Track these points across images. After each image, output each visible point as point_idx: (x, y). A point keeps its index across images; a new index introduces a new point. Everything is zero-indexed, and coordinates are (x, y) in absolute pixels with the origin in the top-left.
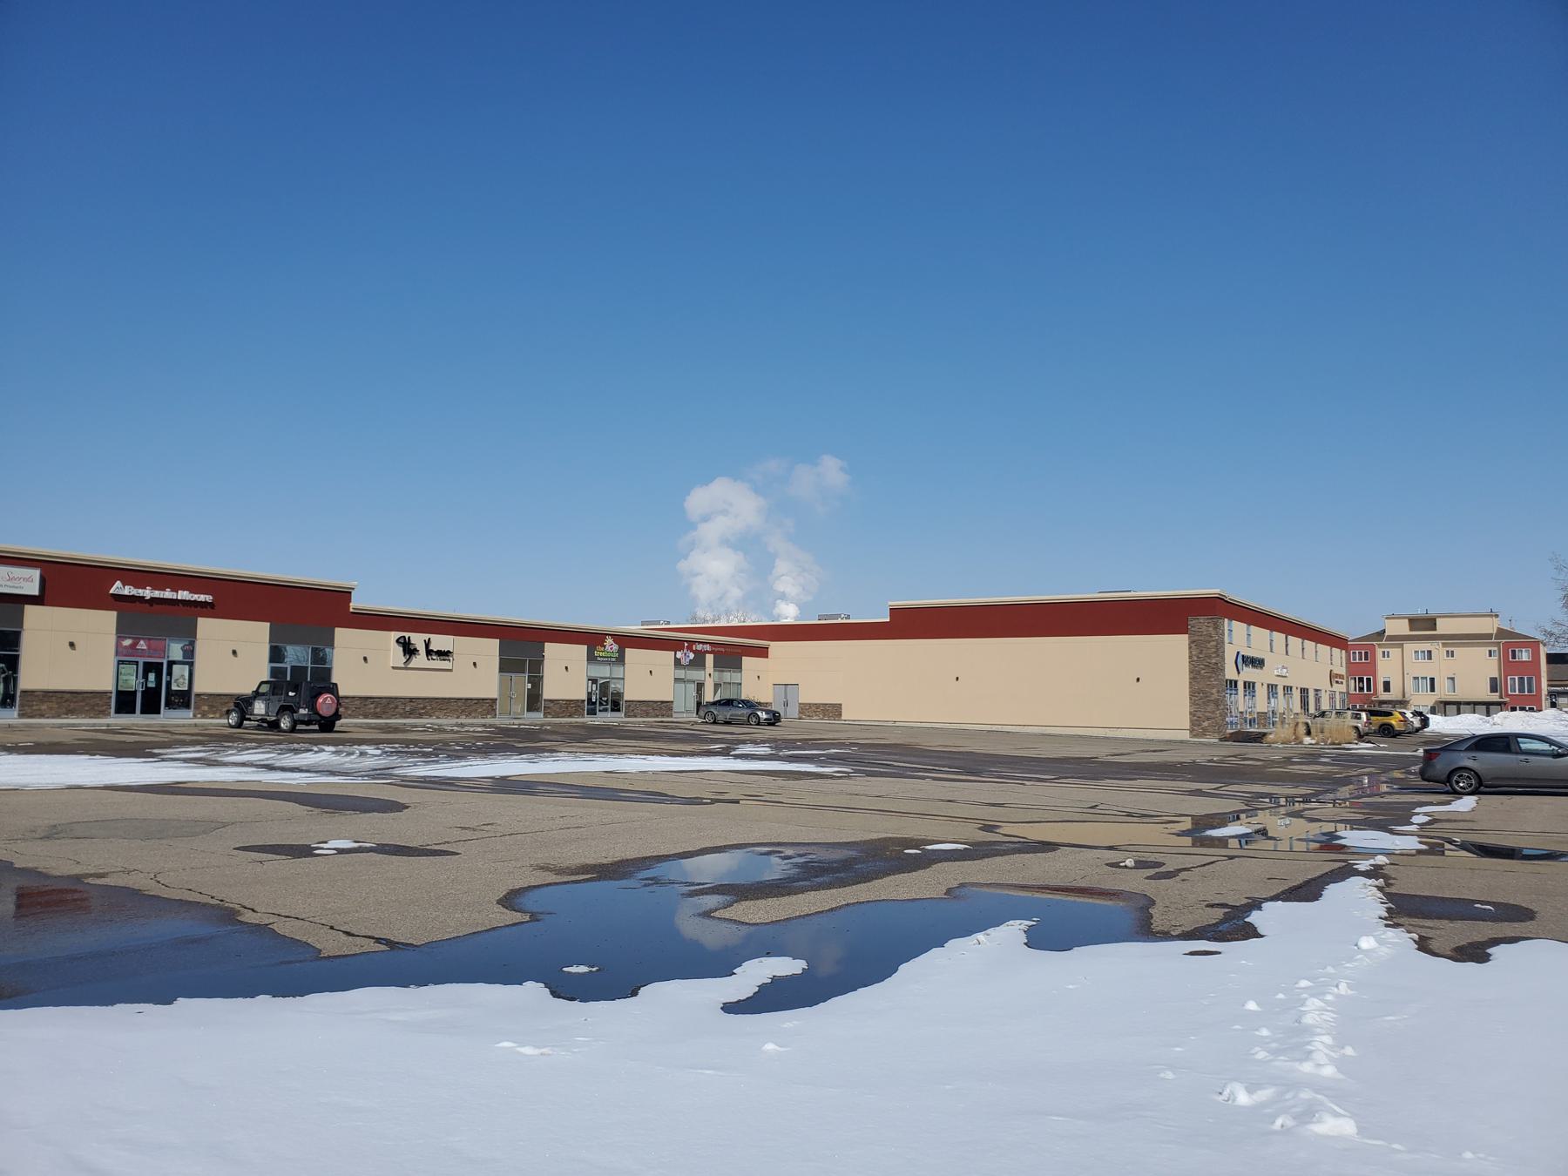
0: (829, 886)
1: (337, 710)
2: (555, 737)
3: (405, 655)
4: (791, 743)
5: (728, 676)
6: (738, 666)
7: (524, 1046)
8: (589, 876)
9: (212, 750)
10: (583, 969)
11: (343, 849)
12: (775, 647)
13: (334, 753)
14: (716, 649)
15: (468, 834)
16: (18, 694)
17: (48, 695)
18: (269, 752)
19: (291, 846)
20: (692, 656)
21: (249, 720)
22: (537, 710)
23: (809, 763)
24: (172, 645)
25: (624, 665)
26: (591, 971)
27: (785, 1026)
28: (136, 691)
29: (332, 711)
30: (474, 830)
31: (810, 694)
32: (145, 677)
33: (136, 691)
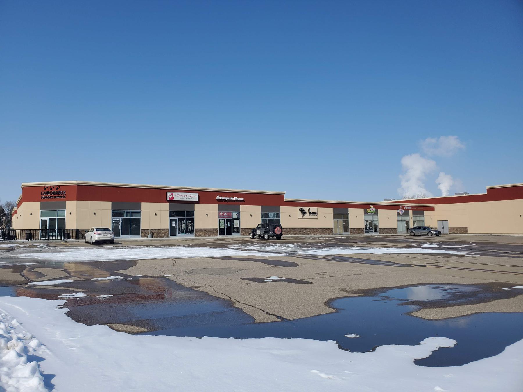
0: (465, 304)
1: (281, 232)
2: (353, 241)
3: (302, 214)
4: (446, 243)
5: (418, 218)
6: (422, 215)
7: (322, 373)
8: (361, 294)
9: (244, 246)
10: (353, 336)
11: (274, 280)
12: (437, 207)
13: (279, 246)
14: (413, 208)
15: (318, 276)
16: (194, 230)
17: (202, 230)
18: (260, 246)
19: (258, 278)
20: (404, 211)
21: (256, 236)
22: (348, 232)
23: (456, 251)
24: (234, 214)
25: (424, 216)
26: (356, 337)
27: (446, 376)
28: (224, 228)
29: (280, 233)
30: (320, 274)
31: (452, 224)
32: (227, 224)
33: (224, 228)
